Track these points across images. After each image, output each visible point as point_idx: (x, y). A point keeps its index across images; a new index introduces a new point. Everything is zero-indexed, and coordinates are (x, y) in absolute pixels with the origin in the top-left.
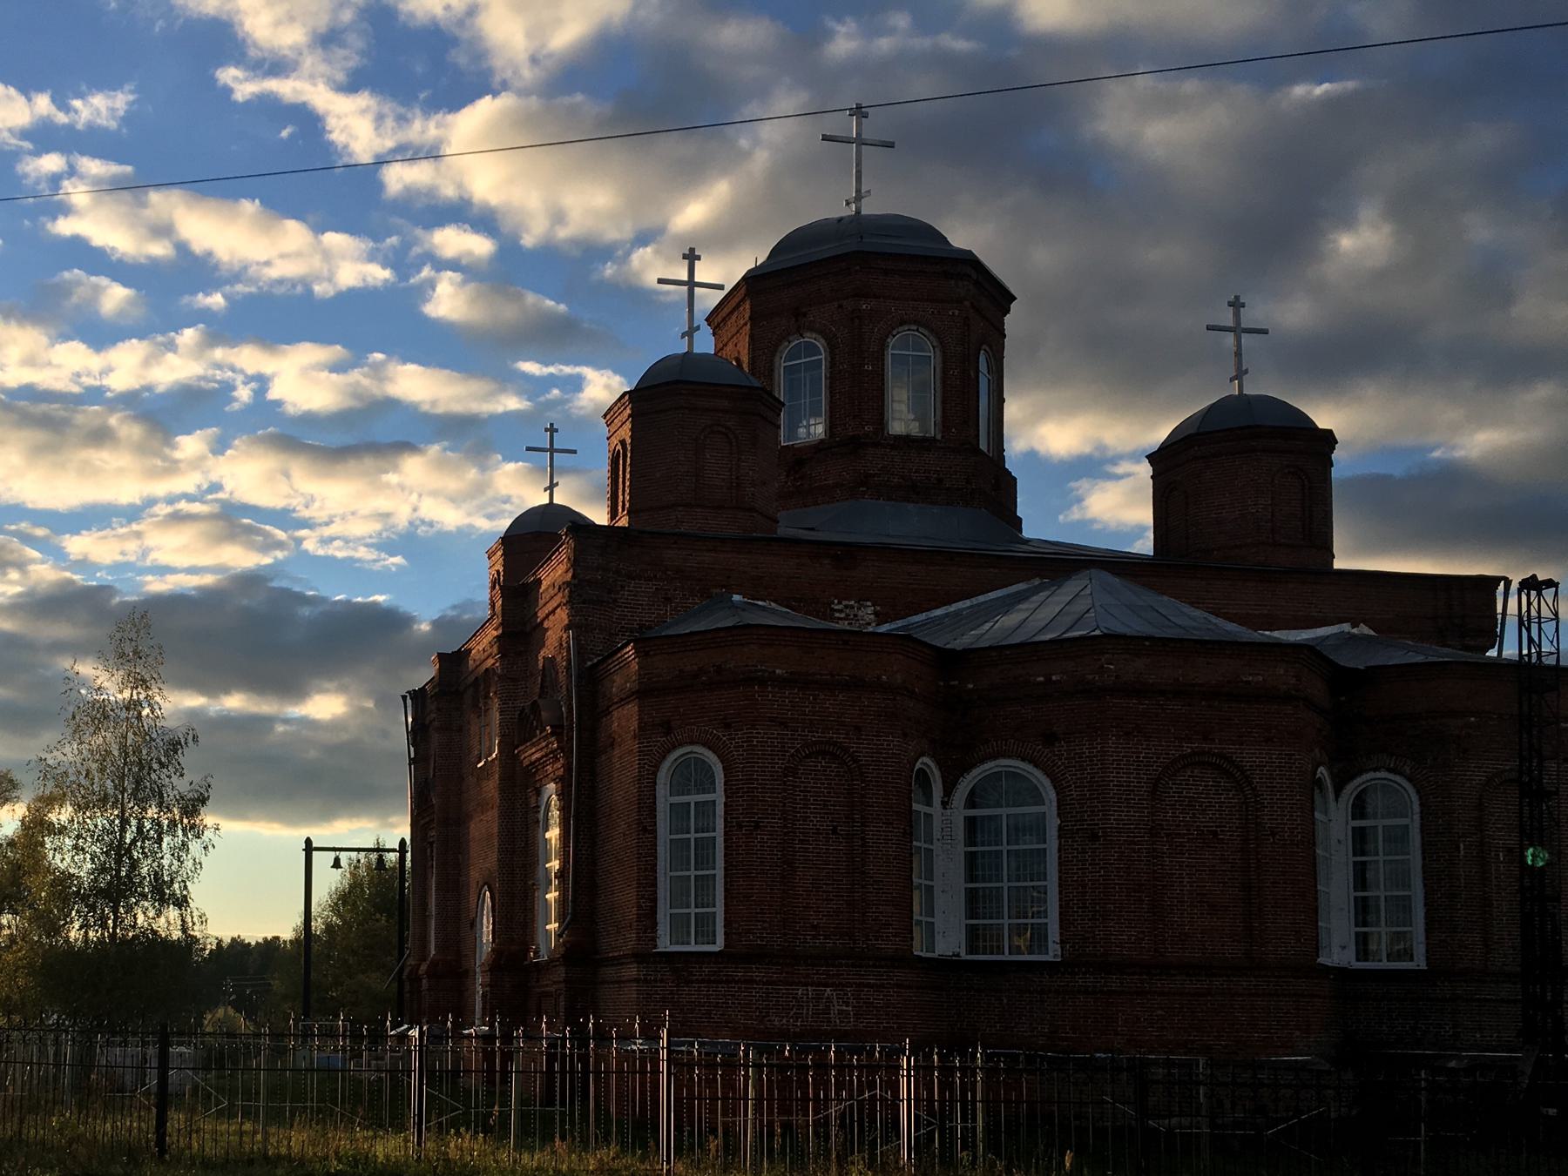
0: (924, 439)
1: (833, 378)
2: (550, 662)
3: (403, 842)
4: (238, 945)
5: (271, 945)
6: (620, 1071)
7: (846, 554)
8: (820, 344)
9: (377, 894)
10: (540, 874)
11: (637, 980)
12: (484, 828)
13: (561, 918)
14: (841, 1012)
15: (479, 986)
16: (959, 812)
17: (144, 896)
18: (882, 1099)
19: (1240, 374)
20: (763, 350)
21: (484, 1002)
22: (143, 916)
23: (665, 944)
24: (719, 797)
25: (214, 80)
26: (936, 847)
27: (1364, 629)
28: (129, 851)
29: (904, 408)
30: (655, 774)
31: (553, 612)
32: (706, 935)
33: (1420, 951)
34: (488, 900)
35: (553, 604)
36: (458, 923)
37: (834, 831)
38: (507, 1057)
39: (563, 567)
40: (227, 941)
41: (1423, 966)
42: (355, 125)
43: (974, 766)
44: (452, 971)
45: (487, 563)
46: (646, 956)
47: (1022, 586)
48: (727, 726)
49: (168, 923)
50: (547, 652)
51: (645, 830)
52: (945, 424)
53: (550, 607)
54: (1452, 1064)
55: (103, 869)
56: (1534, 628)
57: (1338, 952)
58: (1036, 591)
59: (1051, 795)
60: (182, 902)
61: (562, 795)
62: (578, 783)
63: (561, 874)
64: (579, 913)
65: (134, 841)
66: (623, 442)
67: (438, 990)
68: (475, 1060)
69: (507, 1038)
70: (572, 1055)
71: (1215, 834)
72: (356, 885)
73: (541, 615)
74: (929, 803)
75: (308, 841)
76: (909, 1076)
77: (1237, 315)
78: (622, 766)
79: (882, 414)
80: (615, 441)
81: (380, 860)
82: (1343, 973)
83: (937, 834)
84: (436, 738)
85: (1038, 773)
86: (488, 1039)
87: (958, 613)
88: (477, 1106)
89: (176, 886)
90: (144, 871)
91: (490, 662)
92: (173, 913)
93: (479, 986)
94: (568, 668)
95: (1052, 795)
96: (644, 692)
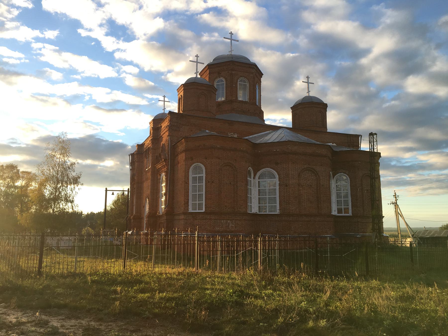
0: (245, 102)
1: (226, 87)
2: (164, 145)
3: (128, 189)
4: (92, 214)
5: (99, 214)
6: (184, 244)
7: (231, 123)
8: (224, 80)
9: (123, 203)
10: (160, 194)
11: (184, 219)
12: (147, 186)
13: (165, 205)
14: (232, 226)
15: (145, 221)
16: (257, 180)
17: (62, 200)
18: (254, 250)
19: (309, 92)
20: (212, 80)
21: (146, 225)
22: (62, 205)
23: (190, 210)
24: (204, 175)
25: (77, 31)
26: (252, 188)
27: (334, 144)
28: (59, 189)
29: (241, 95)
30: (189, 170)
31: (165, 133)
32: (200, 208)
33: (350, 211)
34: (148, 201)
35: (165, 131)
36: (140, 207)
37: (230, 183)
38: (152, 240)
39: (167, 122)
40: (89, 213)
41: (351, 215)
42: (109, 43)
43: (260, 170)
44: (139, 217)
45: (149, 125)
46: (186, 213)
47: (268, 132)
48: (206, 158)
49: (69, 208)
50: (163, 143)
51: (186, 183)
52: (250, 99)
53: (164, 132)
54: (358, 236)
55: (51, 194)
56: (372, 143)
57: (334, 212)
58: (272, 132)
59: (277, 176)
60: (72, 202)
61: (166, 176)
62: (170, 172)
63: (165, 194)
64: (169, 203)
65: (60, 187)
66: (181, 96)
67: (135, 222)
68: (143, 242)
69: (152, 235)
70: (170, 239)
71: (311, 186)
72: (118, 199)
73: (162, 134)
74: (251, 178)
75: (106, 189)
76: (260, 243)
77: (308, 80)
78: (181, 167)
79: (237, 96)
80: (179, 95)
81: (123, 193)
82: (335, 216)
83: (252, 185)
84: (136, 164)
85: (274, 171)
86: (146, 234)
87: (255, 137)
88: (142, 255)
89: (71, 198)
90: (63, 194)
91: (150, 145)
92: (69, 204)
93: (145, 221)
94: (168, 146)
95: (277, 176)
96: (186, 151)
